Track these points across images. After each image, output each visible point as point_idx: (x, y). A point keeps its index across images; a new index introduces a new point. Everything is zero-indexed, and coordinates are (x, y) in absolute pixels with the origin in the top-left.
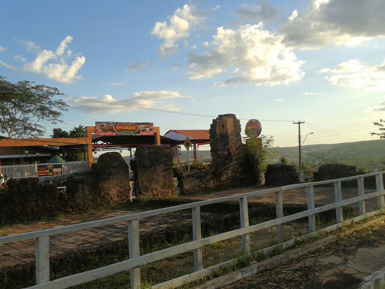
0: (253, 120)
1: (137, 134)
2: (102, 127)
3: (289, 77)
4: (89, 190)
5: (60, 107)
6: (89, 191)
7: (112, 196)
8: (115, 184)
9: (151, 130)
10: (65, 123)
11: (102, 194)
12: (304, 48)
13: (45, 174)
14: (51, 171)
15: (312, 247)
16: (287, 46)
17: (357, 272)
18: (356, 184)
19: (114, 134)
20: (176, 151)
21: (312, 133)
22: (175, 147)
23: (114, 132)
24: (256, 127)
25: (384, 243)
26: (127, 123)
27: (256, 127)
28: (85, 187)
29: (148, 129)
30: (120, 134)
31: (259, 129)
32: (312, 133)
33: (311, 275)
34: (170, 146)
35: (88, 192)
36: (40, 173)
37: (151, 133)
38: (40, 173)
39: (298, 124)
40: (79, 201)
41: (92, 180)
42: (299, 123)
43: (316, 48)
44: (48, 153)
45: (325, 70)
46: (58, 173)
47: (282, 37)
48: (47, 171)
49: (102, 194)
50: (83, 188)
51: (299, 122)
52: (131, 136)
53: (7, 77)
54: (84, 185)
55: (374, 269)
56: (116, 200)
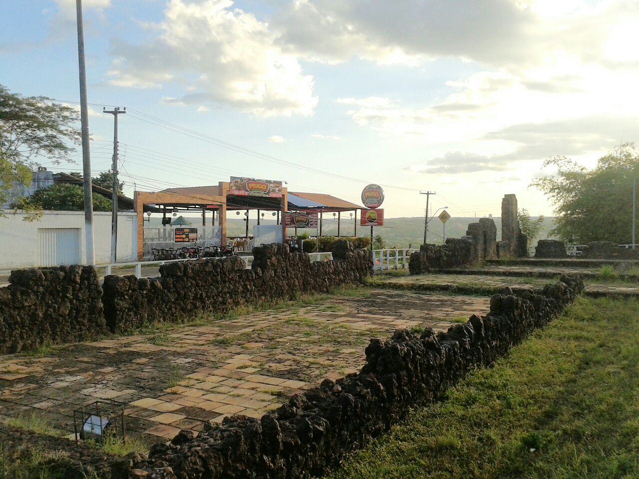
0: (373, 185)
1: (267, 196)
2: (236, 184)
3: (293, 105)
5: (76, 139)
9: (279, 191)
10: (78, 165)
12: (314, 58)
13: (182, 240)
14: (187, 236)
15: (612, 348)
16: (285, 50)
17: (223, 379)
19: (247, 194)
20: (316, 220)
22: (313, 215)
23: (247, 191)
24: (264, 187)
26: (259, 180)
27: (264, 187)
29: (277, 189)
30: (252, 193)
31: (382, 197)
34: (306, 213)
36: (177, 238)
37: (279, 195)
38: (177, 238)
39: (426, 195)
42: (428, 194)
43: (333, 62)
45: (347, 101)
46: (193, 240)
47: (278, 34)
48: (184, 236)
51: (428, 192)
52: (262, 197)
53: (10, 89)
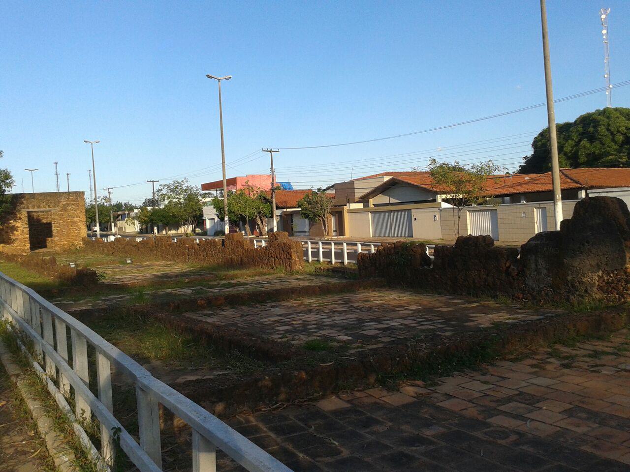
4: (547, 267)
6: (546, 269)
7: (589, 288)
8: (594, 263)
11: (569, 278)
18: (49, 195)
21: (208, 76)
25: (626, 165)
28: (540, 261)
32: (208, 76)
33: (341, 396)
35: (545, 271)
40: (530, 283)
41: (551, 250)
44: (561, 227)
49: (569, 278)
50: (536, 262)
54: (538, 257)
55: (146, 452)
56: (597, 296)
